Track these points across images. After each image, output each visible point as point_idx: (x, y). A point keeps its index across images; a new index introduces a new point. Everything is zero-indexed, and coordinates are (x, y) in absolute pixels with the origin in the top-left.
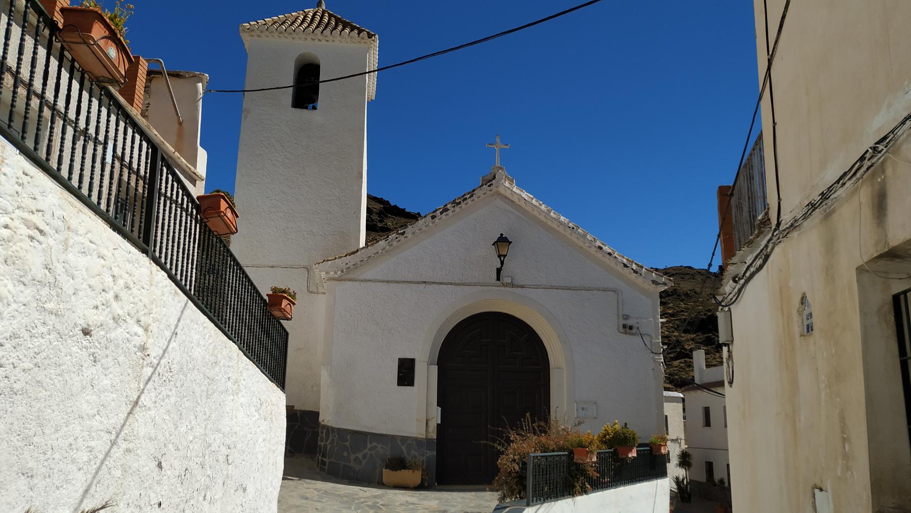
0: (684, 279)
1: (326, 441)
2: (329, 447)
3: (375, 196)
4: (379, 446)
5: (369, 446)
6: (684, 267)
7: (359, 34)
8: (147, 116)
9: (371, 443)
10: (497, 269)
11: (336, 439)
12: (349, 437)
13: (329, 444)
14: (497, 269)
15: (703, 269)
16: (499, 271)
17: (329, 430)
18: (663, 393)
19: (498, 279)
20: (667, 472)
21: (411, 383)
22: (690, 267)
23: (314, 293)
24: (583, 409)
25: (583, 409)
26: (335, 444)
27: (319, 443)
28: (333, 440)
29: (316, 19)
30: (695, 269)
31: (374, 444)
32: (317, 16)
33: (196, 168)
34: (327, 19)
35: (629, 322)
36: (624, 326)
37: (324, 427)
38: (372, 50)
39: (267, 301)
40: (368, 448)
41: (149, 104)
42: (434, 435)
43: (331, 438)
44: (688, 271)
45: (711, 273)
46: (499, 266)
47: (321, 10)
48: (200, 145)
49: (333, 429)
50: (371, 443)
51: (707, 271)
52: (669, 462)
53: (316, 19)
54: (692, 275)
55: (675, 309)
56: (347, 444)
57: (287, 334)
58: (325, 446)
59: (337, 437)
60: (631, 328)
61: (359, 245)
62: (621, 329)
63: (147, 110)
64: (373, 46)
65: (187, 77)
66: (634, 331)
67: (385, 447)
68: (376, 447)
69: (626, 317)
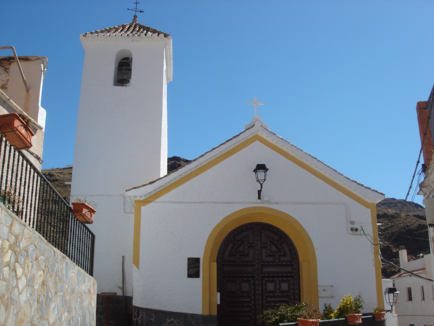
0: (391, 207)
1: (138, 317)
2: (139, 321)
3: (187, 159)
4: (176, 321)
5: (168, 321)
6: (390, 198)
7: (158, 35)
8: (7, 88)
9: (170, 319)
10: (258, 191)
11: (144, 316)
12: (153, 315)
13: (140, 319)
14: (258, 191)
15: (402, 200)
16: (259, 192)
17: (139, 309)
18: (377, 224)
19: (259, 198)
20: (300, 166)
21: (197, 275)
22: (393, 199)
23: (129, 213)
24: (324, 290)
25: (324, 290)
26: (144, 320)
27: (133, 319)
28: (142, 317)
29: (131, 29)
30: (397, 200)
31: (172, 319)
32: (132, 27)
33: (37, 121)
34: (138, 28)
35: (354, 226)
36: (352, 229)
37: (136, 307)
38: (168, 45)
39: (72, 208)
40: (168, 322)
41: (8, 80)
42: (215, 313)
43: (141, 315)
44: (393, 201)
45: (407, 202)
46: (259, 189)
47: (135, 24)
48: (42, 106)
49: (142, 309)
50: (170, 319)
51: (405, 201)
52: (116, 293)
53: (131, 29)
54: (395, 204)
55: (386, 226)
56: (153, 319)
57: (93, 236)
58: (137, 321)
59: (145, 314)
60: (356, 230)
61: (160, 176)
62: (350, 232)
63: (7, 84)
64: (168, 43)
65: (33, 60)
66: (358, 232)
67: (180, 321)
68: (173, 322)
69: (352, 223)
